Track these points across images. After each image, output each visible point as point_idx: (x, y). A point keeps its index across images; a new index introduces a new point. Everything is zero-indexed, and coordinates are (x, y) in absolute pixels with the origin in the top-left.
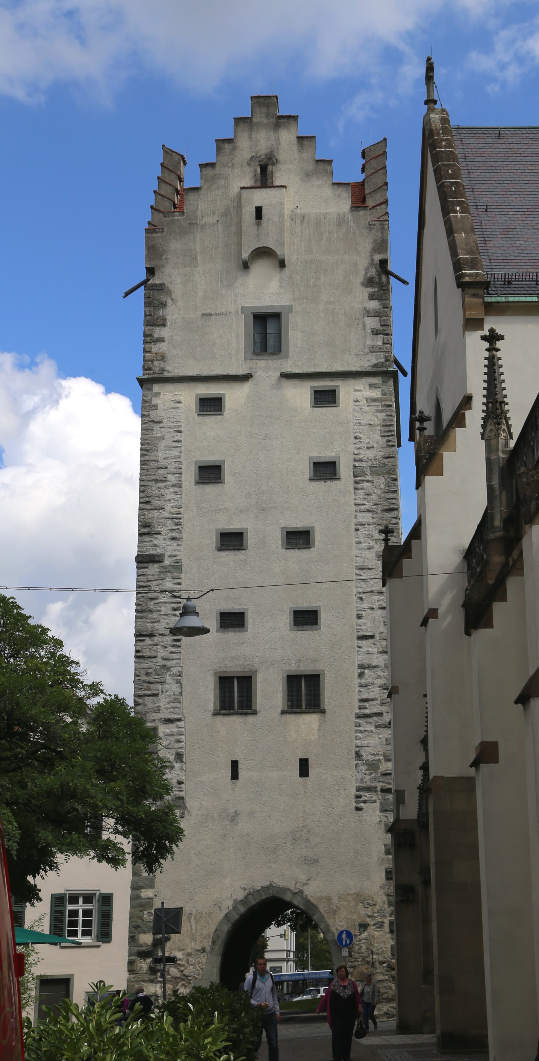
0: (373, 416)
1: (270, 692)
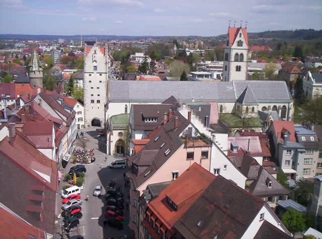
0: (105, 77)
1: (96, 101)
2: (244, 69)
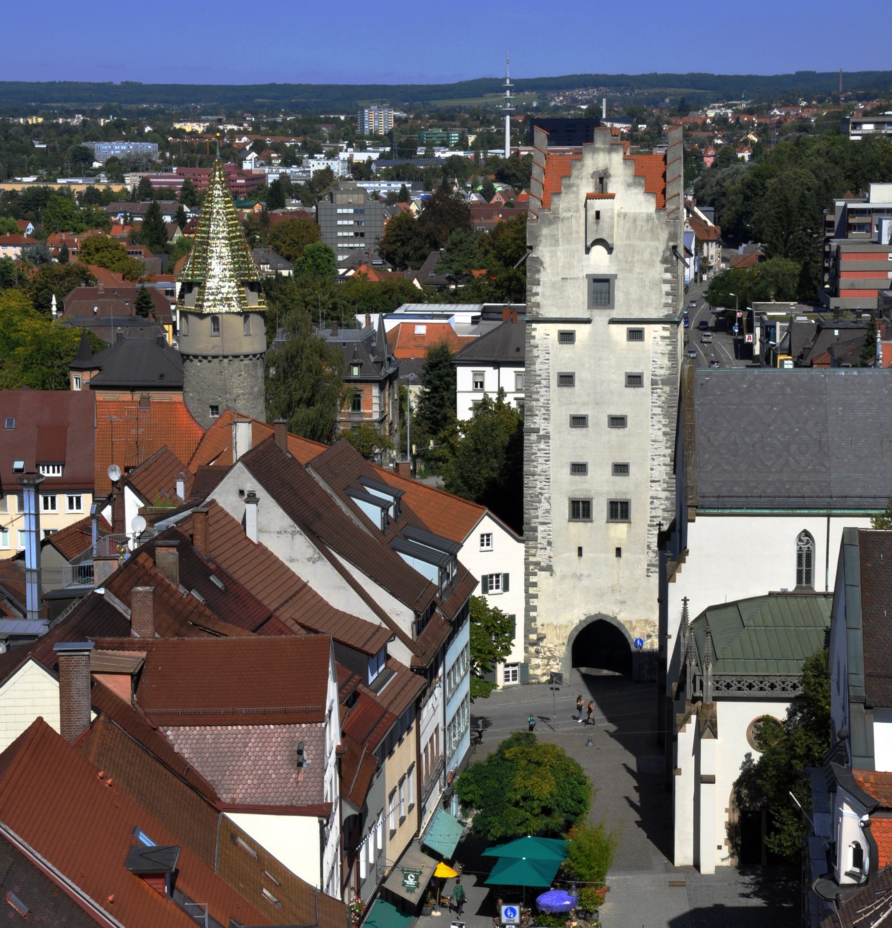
1: (600, 510)
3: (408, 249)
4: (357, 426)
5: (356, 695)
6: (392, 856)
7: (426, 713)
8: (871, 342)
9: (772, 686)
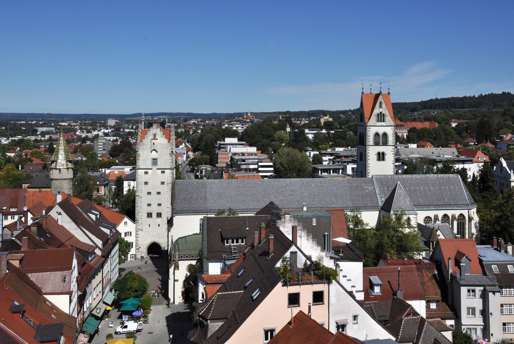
1: (154, 215)
2: (390, 157)
3: (116, 153)
4: (98, 196)
5: (85, 263)
6: (94, 305)
7: (105, 267)
8: (222, 174)
9: (192, 257)
